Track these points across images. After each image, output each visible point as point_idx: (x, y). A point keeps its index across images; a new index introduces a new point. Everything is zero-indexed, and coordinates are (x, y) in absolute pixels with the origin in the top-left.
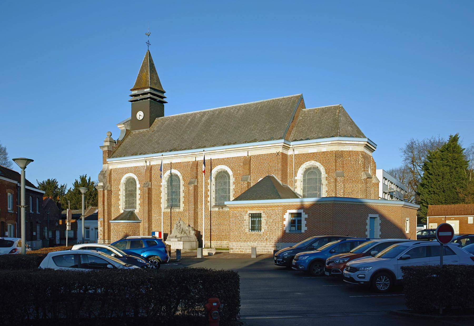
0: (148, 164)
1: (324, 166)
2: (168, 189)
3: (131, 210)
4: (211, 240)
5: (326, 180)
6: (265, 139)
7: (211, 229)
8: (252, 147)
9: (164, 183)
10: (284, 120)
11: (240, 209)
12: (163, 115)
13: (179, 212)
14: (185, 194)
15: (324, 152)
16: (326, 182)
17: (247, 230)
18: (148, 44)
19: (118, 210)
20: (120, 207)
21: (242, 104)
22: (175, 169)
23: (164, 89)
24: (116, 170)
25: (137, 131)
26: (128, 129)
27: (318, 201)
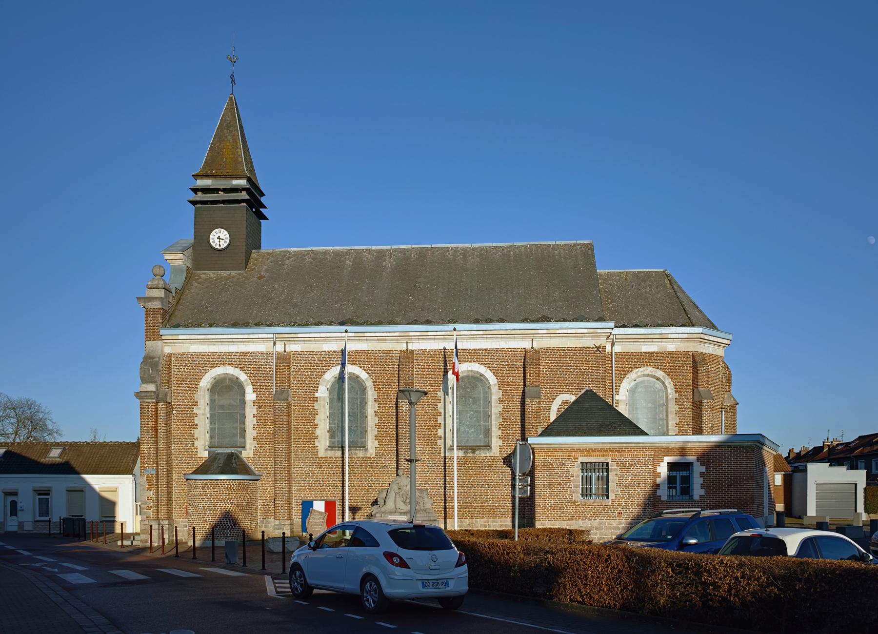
0: (279, 348)
1: (672, 378)
2: (331, 408)
3: (230, 450)
4: (445, 518)
5: (676, 403)
6: (566, 317)
7: (445, 495)
8: (545, 331)
9: (323, 392)
10: (562, 285)
11: (561, 454)
12: (259, 248)
13: (363, 459)
14: (380, 419)
15: (671, 353)
16: (677, 408)
17: (578, 497)
19: (192, 451)
20: (196, 443)
21: (469, 245)
22: (353, 363)
24: (184, 357)
25: (211, 274)
26: (190, 266)
27: (724, 442)
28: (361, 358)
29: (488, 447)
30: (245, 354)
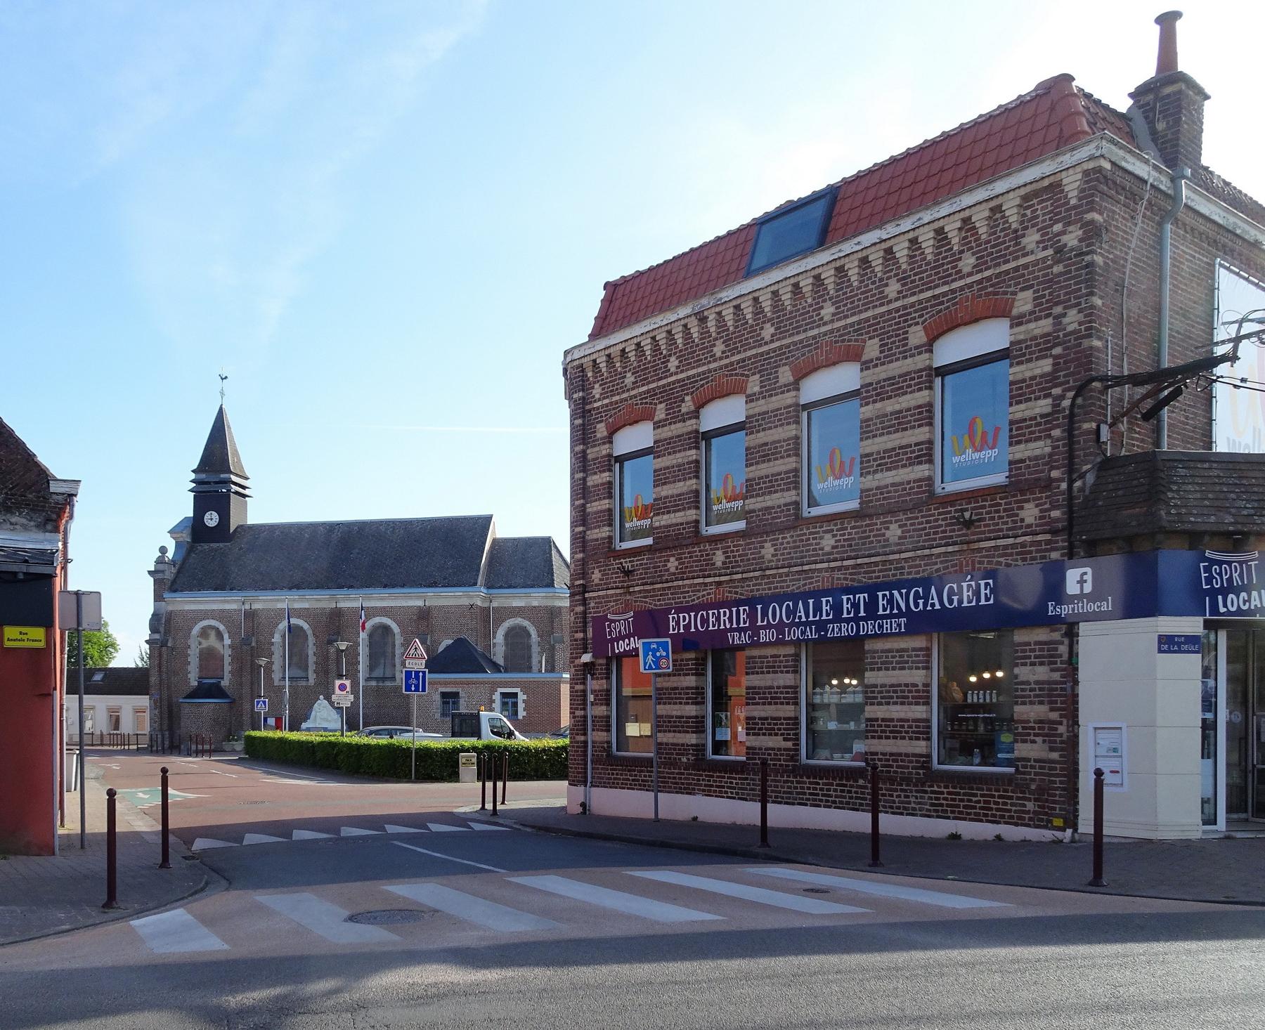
0: (247, 607)
13: (307, 687)
17: (438, 716)
18: (222, 394)
19: (187, 681)
23: (248, 474)
24: (183, 613)
25: (206, 546)
28: (300, 613)
29: (393, 678)
30: (223, 611)
